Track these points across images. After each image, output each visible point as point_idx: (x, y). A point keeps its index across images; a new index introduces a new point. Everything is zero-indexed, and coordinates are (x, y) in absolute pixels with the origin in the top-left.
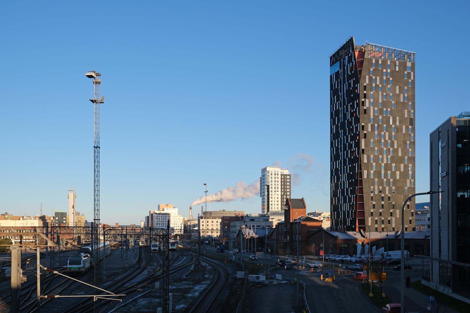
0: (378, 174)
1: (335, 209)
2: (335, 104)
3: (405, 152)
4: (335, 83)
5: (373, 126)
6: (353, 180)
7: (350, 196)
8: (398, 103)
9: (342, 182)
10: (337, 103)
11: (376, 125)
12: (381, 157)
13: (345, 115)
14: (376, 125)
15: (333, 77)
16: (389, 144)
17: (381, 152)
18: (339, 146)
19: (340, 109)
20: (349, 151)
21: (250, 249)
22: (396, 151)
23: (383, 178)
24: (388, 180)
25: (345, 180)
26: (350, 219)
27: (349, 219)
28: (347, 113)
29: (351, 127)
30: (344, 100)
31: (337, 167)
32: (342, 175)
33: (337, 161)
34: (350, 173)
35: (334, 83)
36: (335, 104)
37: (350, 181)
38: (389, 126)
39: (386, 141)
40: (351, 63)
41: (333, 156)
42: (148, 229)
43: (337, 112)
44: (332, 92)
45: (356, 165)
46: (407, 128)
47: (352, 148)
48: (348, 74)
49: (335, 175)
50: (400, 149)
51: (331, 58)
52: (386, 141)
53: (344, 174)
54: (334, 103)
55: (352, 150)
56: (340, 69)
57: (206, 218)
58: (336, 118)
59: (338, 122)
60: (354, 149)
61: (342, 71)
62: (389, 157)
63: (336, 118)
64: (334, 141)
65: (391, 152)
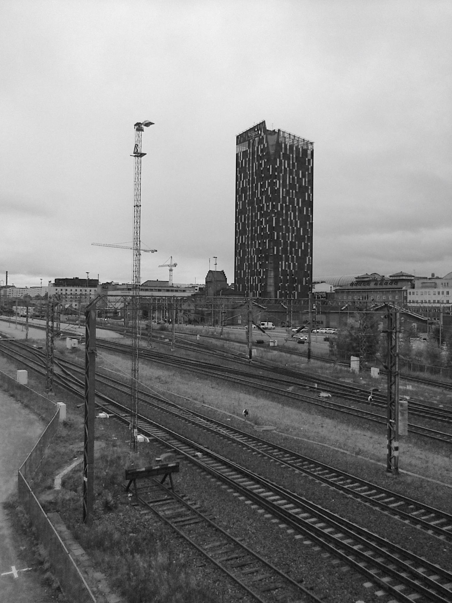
0: (285, 251)
1: (238, 268)
2: (241, 182)
3: (305, 231)
4: (242, 161)
5: (282, 205)
6: (263, 255)
7: (259, 270)
8: (301, 186)
10: (245, 180)
11: (284, 205)
12: (287, 234)
13: (254, 194)
14: (284, 205)
15: (239, 155)
16: (290, 260)
17: (288, 230)
19: (248, 186)
20: (259, 213)
22: (298, 230)
23: (295, 205)
24: (293, 257)
26: (259, 292)
27: (258, 292)
28: (257, 191)
29: (261, 205)
30: (253, 179)
31: (244, 242)
33: (244, 236)
34: (260, 233)
35: (240, 162)
36: (241, 182)
37: (259, 256)
38: (294, 207)
39: (291, 221)
40: (262, 145)
43: (244, 190)
44: (238, 169)
45: (266, 241)
46: (307, 210)
47: (262, 224)
48: (258, 155)
50: (302, 229)
51: (237, 137)
52: (291, 221)
53: (252, 249)
54: (240, 180)
55: (262, 227)
56: (249, 148)
59: (245, 199)
60: (265, 226)
61: (251, 151)
62: (294, 235)
64: (240, 217)
65: (295, 232)
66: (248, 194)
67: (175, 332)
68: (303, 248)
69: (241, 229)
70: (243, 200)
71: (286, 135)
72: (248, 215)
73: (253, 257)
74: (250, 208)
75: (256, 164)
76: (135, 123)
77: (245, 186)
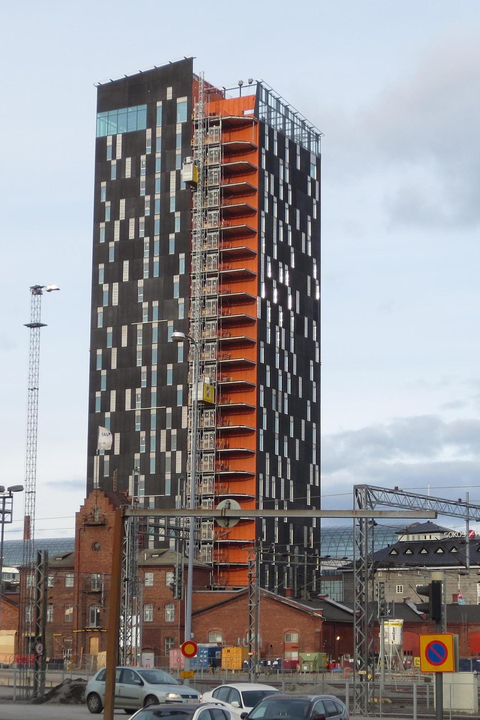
2: (117, 224)
9: (153, 455)
18: (143, 178)
21: (272, 583)
25: (168, 448)
32: (153, 433)
35: (114, 163)
36: (117, 224)
41: (104, 373)
42: (332, 586)
49: (109, 389)
53: (163, 433)
56: (151, 123)
57: (382, 590)
58: (126, 264)
63: (126, 264)
66: (146, 261)
67: (398, 587)
68: (303, 422)
69: (114, 366)
70: (126, 277)
71: (272, 103)
72: (148, 328)
73: (168, 454)
74: (155, 304)
75: (169, 433)
76: (161, 718)
77: (132, 236)
